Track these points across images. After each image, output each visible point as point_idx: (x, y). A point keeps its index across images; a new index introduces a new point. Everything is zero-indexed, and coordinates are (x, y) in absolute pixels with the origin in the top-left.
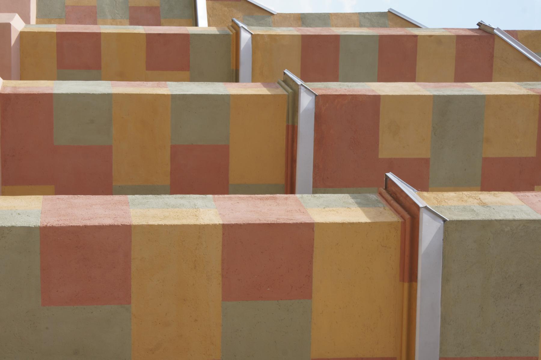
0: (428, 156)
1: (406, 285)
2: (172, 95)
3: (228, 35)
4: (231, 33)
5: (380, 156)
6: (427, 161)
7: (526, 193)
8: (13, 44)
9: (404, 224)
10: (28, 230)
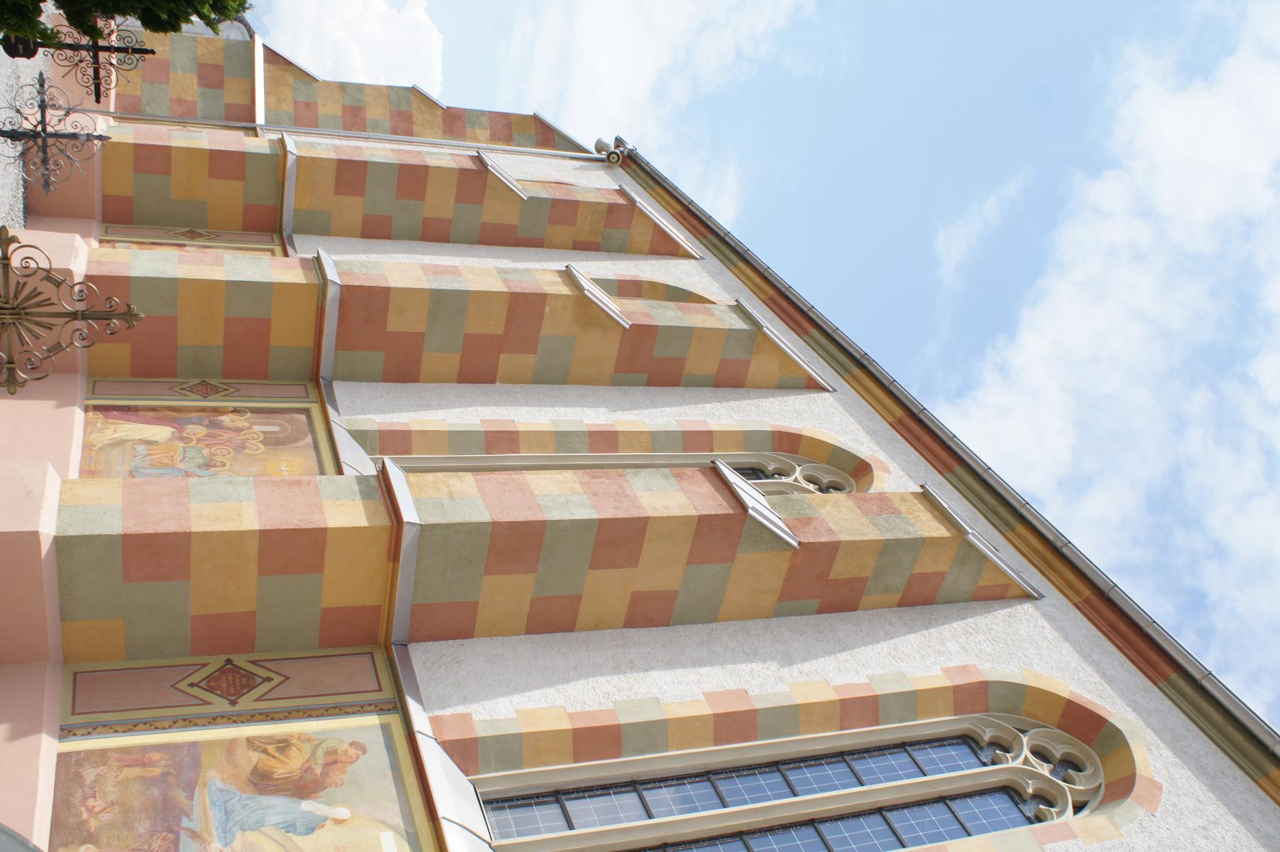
0: (424, 331)
1: (391, 564)
2: (228, 282)
3: (278, 155)
4: (280, 153)
5: (388, 330)
6: (422, 335)
7: (481, 475)
8: (46, 554)
9: (392, 526)
10: (110, 538)
